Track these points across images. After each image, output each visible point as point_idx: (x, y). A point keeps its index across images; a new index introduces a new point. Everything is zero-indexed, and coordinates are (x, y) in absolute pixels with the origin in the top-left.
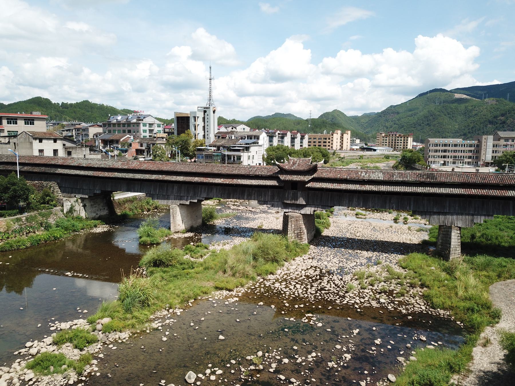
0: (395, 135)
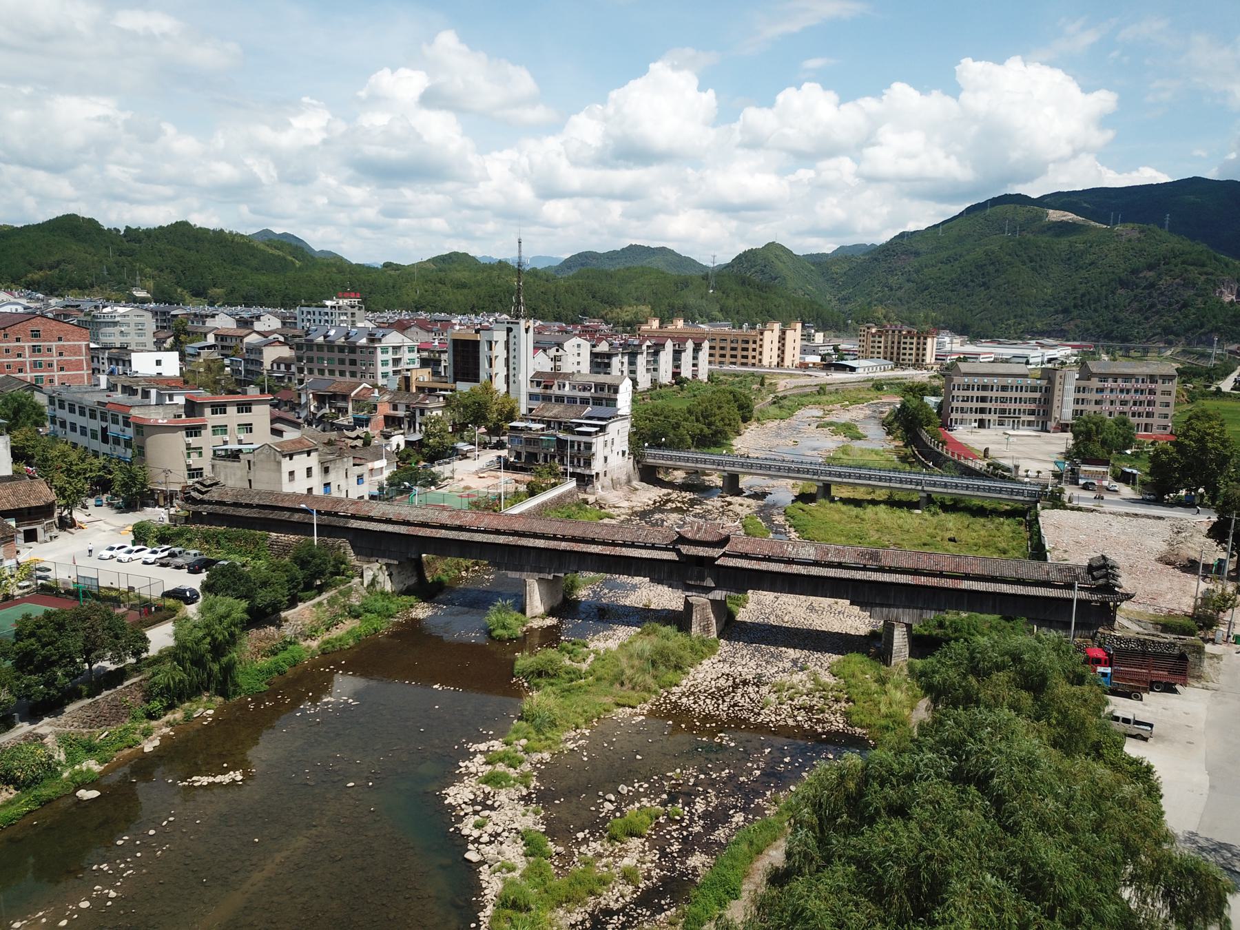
0: (900, 332)
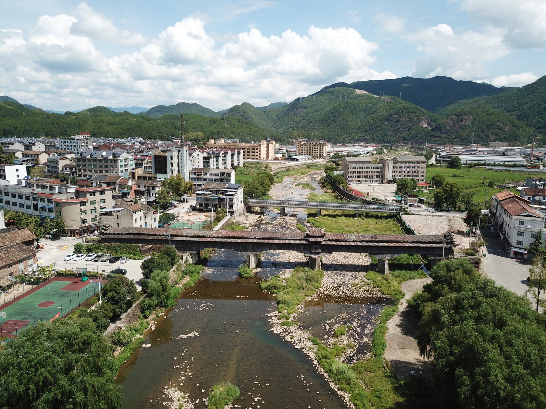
0: (313, 144)
